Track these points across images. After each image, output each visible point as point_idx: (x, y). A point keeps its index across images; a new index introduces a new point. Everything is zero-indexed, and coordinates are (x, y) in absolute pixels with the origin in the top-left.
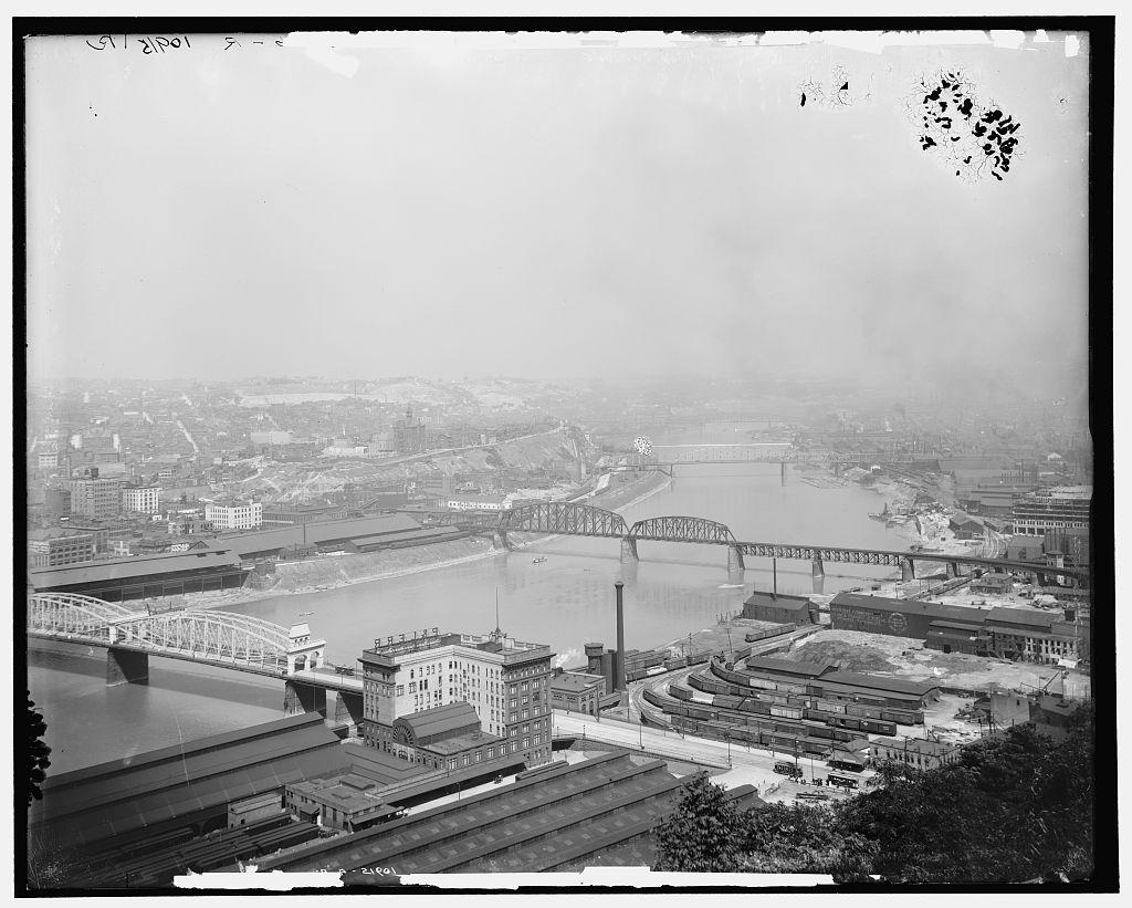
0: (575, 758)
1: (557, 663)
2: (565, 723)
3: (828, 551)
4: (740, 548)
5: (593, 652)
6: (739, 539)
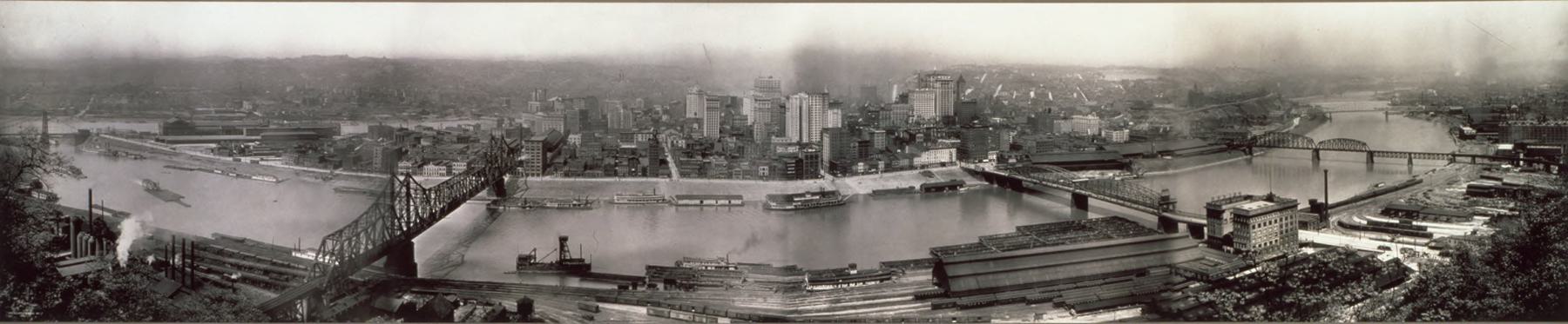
0: (1310, 251)
1: (1299, 207)
2: (1304, 235)
3: (1415, 154)
4: (1371, 154)
5: (1313, 202)
6: (1372, 149)
